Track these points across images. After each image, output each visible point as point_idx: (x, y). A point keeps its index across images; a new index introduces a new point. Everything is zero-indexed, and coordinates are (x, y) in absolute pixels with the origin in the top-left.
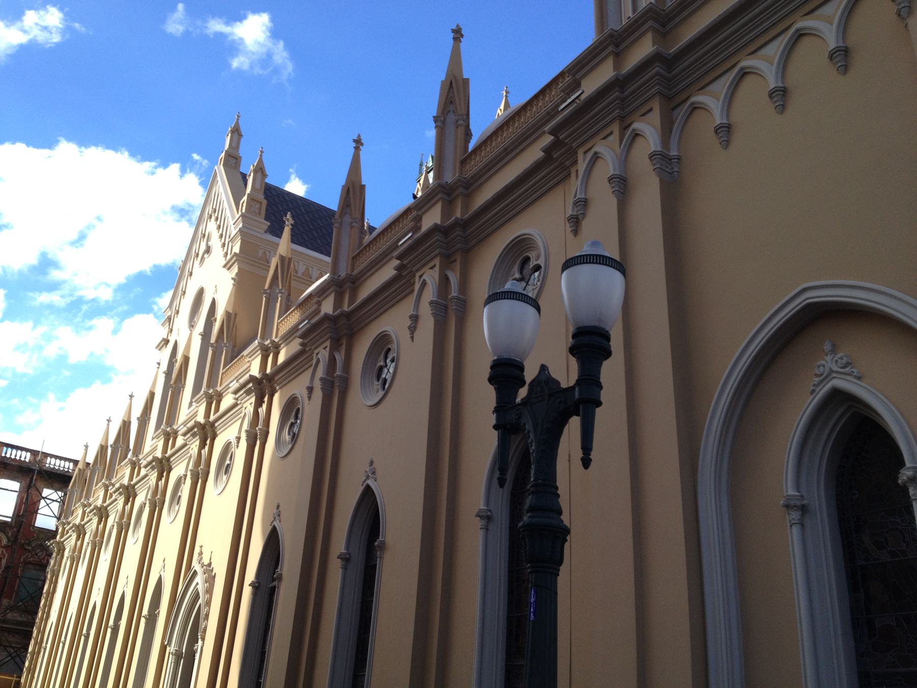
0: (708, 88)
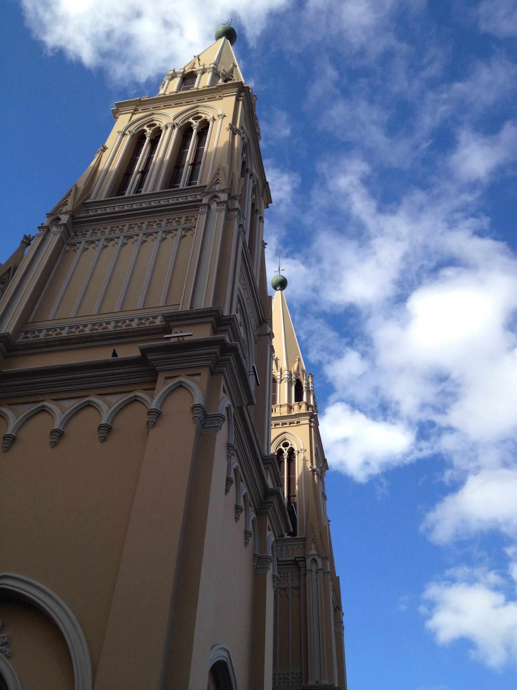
0: (14, 407)
